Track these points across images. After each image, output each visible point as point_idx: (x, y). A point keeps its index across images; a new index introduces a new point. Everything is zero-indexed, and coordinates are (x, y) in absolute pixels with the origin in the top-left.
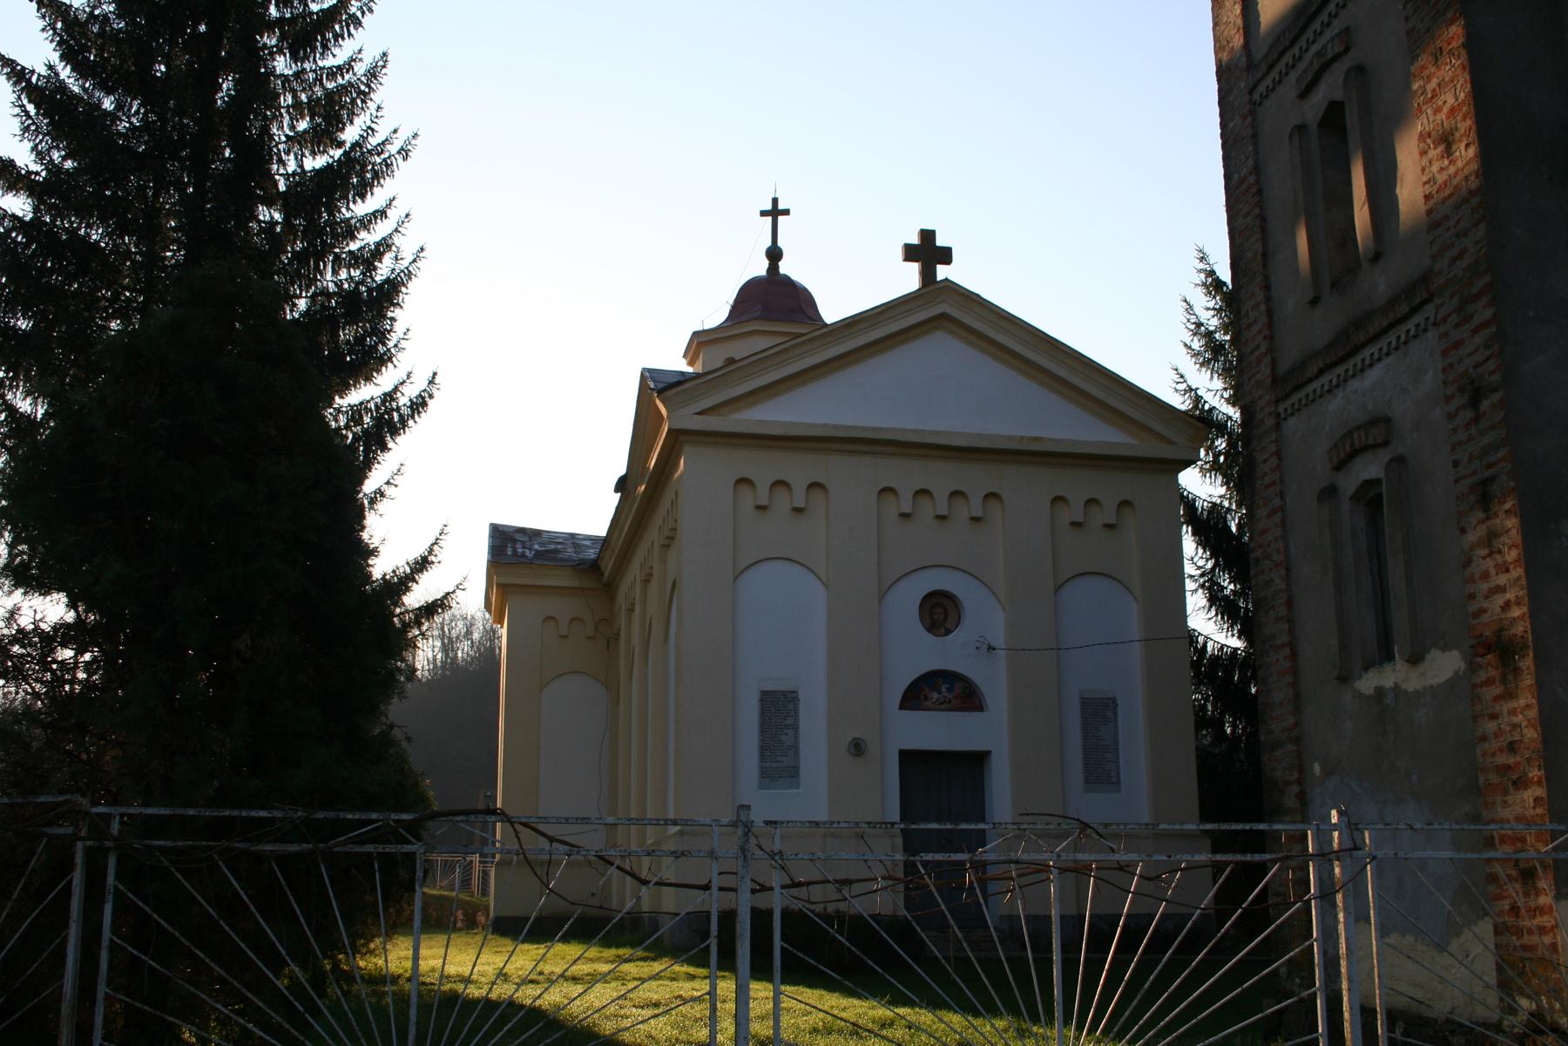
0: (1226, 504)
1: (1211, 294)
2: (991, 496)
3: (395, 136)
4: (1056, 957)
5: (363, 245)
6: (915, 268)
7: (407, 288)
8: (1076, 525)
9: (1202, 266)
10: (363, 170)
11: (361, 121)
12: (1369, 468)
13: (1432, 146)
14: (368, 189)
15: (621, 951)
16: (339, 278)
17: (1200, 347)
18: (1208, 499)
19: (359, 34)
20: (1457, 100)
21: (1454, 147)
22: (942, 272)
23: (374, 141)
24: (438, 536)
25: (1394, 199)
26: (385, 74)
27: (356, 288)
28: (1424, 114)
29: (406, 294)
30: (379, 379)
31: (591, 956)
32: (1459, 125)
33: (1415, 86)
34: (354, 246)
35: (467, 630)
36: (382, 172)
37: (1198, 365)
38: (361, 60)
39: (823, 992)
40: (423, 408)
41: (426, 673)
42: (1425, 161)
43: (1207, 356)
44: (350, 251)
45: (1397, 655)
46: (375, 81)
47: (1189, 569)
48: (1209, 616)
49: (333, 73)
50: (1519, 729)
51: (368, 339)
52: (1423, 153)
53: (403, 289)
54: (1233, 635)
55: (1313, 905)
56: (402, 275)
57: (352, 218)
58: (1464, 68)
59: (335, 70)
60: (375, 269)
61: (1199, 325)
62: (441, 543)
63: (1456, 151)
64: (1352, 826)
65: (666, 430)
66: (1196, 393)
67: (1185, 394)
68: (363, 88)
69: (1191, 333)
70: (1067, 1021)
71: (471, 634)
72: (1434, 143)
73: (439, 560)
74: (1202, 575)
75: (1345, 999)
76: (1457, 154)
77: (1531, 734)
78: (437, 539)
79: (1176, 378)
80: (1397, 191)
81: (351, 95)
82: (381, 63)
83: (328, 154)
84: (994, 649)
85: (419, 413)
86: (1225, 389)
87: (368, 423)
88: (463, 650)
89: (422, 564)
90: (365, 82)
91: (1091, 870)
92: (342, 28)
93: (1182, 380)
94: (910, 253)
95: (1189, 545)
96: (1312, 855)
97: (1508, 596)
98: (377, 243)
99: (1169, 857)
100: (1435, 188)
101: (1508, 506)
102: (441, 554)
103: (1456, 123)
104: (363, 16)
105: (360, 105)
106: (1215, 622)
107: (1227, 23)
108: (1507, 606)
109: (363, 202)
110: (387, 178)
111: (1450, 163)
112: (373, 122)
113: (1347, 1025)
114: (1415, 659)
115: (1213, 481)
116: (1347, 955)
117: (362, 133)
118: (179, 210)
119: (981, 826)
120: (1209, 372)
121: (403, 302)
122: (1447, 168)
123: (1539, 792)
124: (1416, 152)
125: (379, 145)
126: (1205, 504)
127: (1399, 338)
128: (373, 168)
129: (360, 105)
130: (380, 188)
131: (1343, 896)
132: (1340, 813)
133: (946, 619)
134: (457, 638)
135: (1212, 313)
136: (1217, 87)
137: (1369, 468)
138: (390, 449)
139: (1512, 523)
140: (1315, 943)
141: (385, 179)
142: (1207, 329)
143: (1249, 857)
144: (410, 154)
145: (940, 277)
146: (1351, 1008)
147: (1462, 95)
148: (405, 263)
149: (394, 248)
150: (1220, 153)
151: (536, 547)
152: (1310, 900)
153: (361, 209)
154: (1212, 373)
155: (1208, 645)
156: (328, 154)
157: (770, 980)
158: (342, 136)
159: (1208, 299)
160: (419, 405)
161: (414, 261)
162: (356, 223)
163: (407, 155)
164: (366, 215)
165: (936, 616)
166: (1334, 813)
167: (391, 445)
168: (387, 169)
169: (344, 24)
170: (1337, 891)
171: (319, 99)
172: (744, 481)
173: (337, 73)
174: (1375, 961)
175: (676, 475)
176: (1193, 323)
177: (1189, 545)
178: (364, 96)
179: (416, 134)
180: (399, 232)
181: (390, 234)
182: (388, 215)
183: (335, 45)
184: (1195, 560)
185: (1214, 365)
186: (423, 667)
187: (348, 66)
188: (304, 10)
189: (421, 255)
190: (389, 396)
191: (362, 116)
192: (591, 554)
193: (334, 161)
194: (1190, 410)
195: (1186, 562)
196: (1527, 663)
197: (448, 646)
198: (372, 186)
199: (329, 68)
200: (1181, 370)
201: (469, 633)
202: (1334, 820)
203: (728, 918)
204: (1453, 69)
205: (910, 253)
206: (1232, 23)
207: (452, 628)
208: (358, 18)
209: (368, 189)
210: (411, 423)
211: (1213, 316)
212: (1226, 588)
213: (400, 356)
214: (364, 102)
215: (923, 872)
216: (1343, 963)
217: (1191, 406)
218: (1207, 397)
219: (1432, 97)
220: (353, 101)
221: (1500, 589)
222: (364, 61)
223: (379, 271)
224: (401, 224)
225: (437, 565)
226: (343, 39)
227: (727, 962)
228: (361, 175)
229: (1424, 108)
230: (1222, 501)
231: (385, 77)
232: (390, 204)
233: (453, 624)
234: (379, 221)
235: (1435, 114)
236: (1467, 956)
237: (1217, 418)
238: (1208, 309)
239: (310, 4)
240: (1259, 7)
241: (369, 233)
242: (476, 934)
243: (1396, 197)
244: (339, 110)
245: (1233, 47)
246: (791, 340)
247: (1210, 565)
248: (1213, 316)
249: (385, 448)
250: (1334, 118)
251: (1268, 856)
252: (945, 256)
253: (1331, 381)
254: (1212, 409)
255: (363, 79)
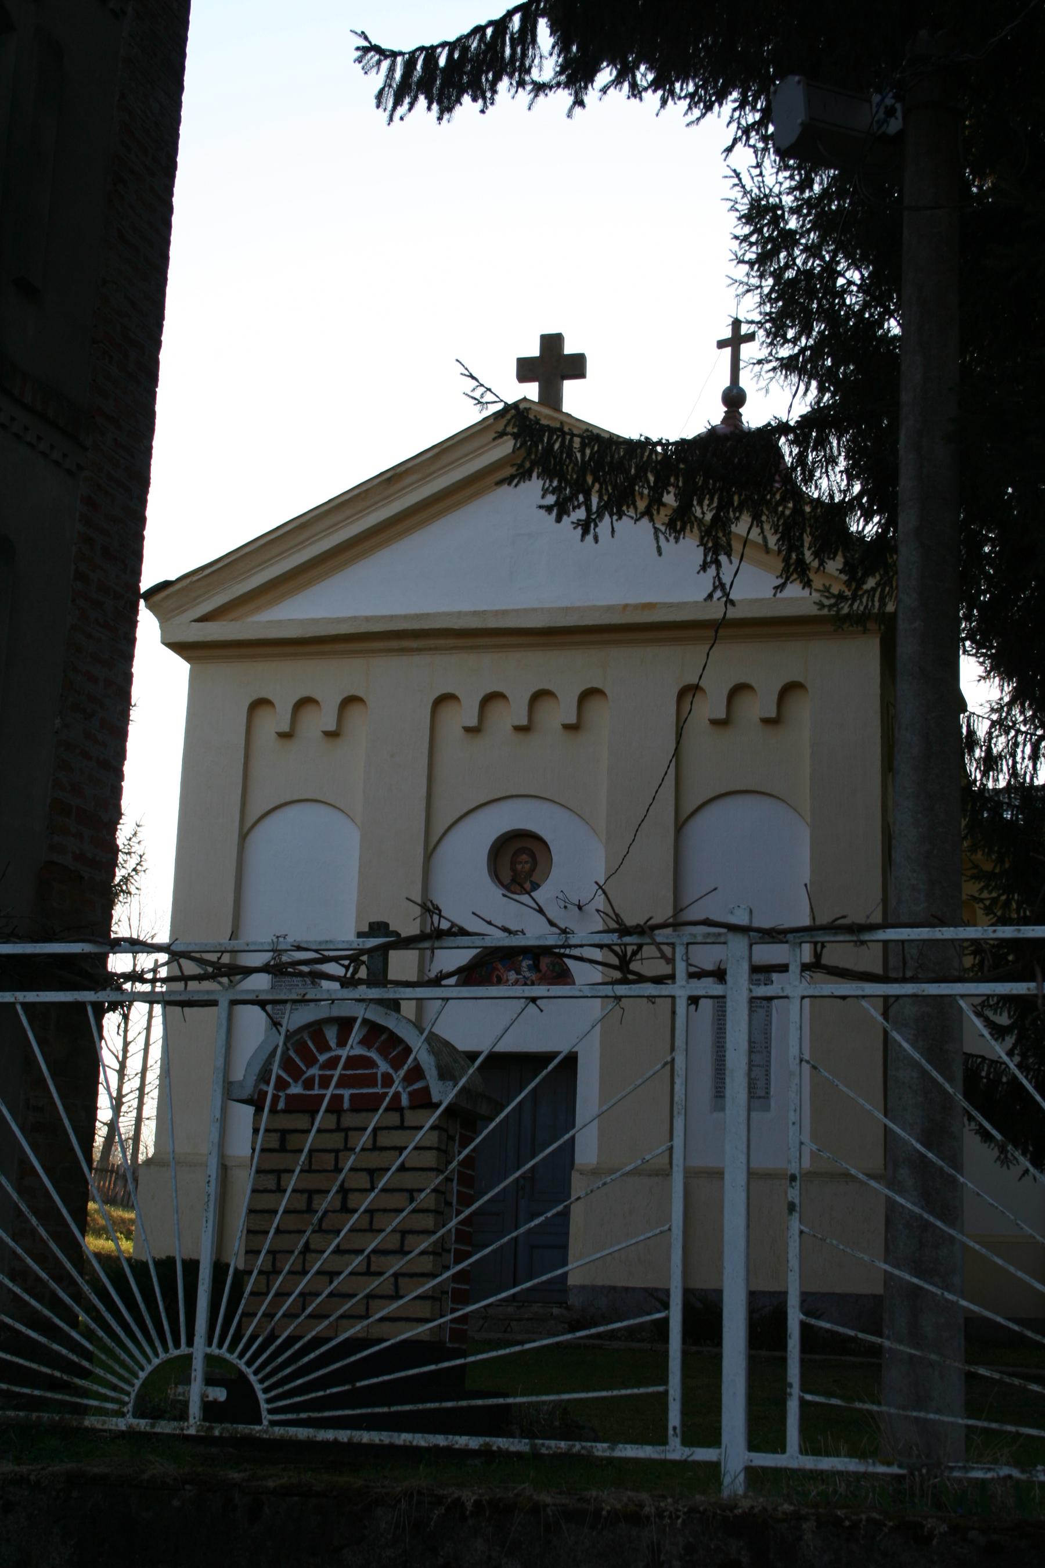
73: (143, 869)
118: (857, 472)
133: (533, 870)
165: (519, 867)
252: (576, 366)
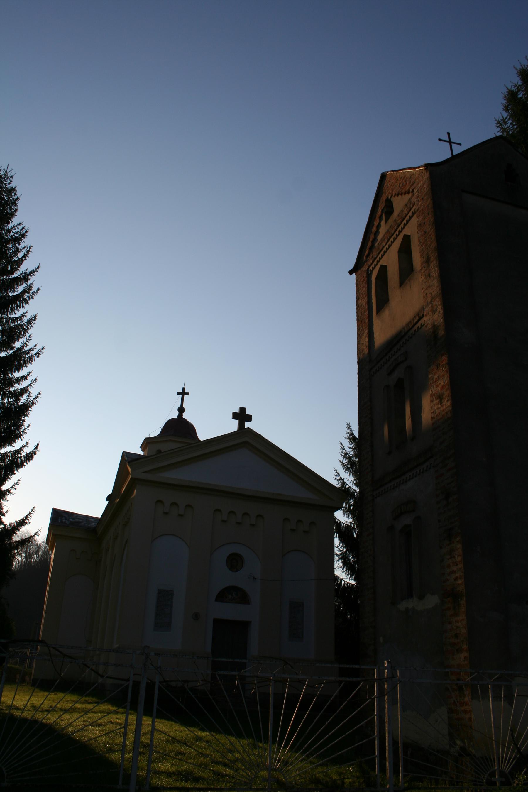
0: (352, 526)
1: (351, 442)
2: (259, 516)
3: (35, 347)
4: (271, 718)
5: (15, 389)
6: (236, 422)
7: (31, 409)
8: (292, 530)
9: (348, 431)
10: (20, 360)
11: (22, 340)
12: (407, 520)
13: (435, 399)
14: (21, 367)
15: (87, 699)
16: (4, 401)
17: (346, 462)
18: (346, 523)
19: (27, 307)
20: (444, 383)
21: (443, 401)
22: (247, 425)
23: (26, 349)
24: (30, 512)
25: (421, 418)
26: (34, 323)
27: (10, 407)
28: (433, 387)
29: (31, 411)
30: (15, 445)
31: (74, 700)
32: (445, 393)
33: (430, 376)
34: (12, 389)
35: (37, 550)
36: (28, 361)
37: (345, 470)
38: (26, 316)
39: (173, 723)
40: (31, 458)
41: (17, 567)
42: (432, 405)
43: (348, 466)
44: (10, 391)
45: (414, 596)
46: (30, 325)
47: (336, 551)
48: (343, 571)
49: (14, 320)
50: (459, 629)
51: (12, 428)
52: (432, 401)
53: (30, 409)
54: (352, 579)
55: (376, 700)
56: (30, 403)
57: (13, 378)
58: (447, 372)
59: (15, 319)
60: (19, 400)
61: (346, 454)
62: (32, 515)
63: (443, 402)
64: (392, 668)
65: (130, 477)
66: (343, 481)
67: (339, 481)
68: (25, 327)
69: (343, 457)
70: (274, 742)
71: (39, 552)
72: (436, 398)
73: (29, 522)
74: (341, 554)
75: (387, 741)
76: (444, 403)
77: (464, 631)
78: (30, 513)
79: (336, 474)
80: (422, 414)
81: (20, 329)
82: (33, 319)
83: (7, 352)
84: (256, 579)
85: (29, 460)
86: (355, 480)
87: (7, 462)
88: (34, 559)
89: (22, 523)
90: (26, 325)
91: (287, 682)
92: (20, 303)
93: (338, 475)
94: (235, 416)
95: (337, 541)
96: (376, 679)
97: (457, 575)
98: (21, 389)
99: (319, 677)
100: (436, 415)
101: (458, 539)
102: (31, 520)
103: (444, 392)
104: (29, 300)
105: (23, 334)
106: (345, 573)
107: (363, 344)
108: (456, 579)
109: (18, 372)
110: (29, 364)
111: (441, 406)
112: (27, 341)
113: (387, 752)
114: (421, 597)
115: (348, 516)
116: (388, 722)
117: (22, 345)
119: (244, 661)
120: (349, 473)
121: (29, 414)
122: (440, 408)
123: (466, 654)
124: (429, 401)
125: (28, 350)
126: (344, 525)
127: (420, 470)
128: (24, 359)
129: (23, 334)
130: (26, 367)
131: (388, 697)
132: (388, 662)
134: (33, 553)
135: (351, 449)
136: (357, 367)
137: (407, 520)
138: (15, 474)
139: (459, 546)
140: (376, 717)
141: (28, 364)
142: (349, 456)
143: (351, 679)
144: (40, 355)
145: (246, 427)
146: (389, 745)
147: (446, 382)
148: (32, 399)
149: (28, 392)
150: (357, 392)
151: (71, 520)
152: (374, 698)
153: (17, 375)
154: (350, 473)
155: (342, 582)
156: (7, 352)
157: (151, 716)
158: (13, 345)
159: (350, 444)
160: (30, 456)
161: (36, 398)
162: (14, 380)
163: (39, 356)
164: (19, 377)
166: (386, 662)
167: (16, 472)
168: (30, 360)
169: (21, 302)
170: (385, 695)
171: (7, 329)
172: (160, 502)
173: (15, 320)
174: (399, 725)
175: (132, 497)
176: (344, 453)
177: (337, 541)
178: (25, 331)
179: (43, 348)
180: (31, 386)
181: (27, 386)
182: (28, 378)
183: (16, 310)
184: (339, 548)
185: (351, 470)
186: (16, 564)
187: (20, 318)
188: (6, 294)
189: (39, 396)
190: (18, 451)
191: (23, 338)
192: (94, 525)
193: (9, 355)
194: (340, 487)
195: (335, 548)
196: (463, 602)
197: (28, 556)
198: (23, 366)
199: (12, 318)
200: (338, 471)
201: (38, 552)
202: (386, 665)
203: (137, 685)
204: (443, 372)
205: (235, 416)
206: (364, 344)
207: (31, 549)
208: (27, 300)
209: (21, 367)
210: (25, 464)
211: (352, 451)
212: (351, 560)
213: (24, 436)
214: (24, 333)
215: (218, 679)
216: (387, 725)
217: (341, 486)
218: (348, 482)
219: (436, 381)
220: (20, 332)
221: (454, 572)
222: (27, 317)
223: (21, 401)
224: (32, 382)
225: (28, 524)
226: (20, 308)
227: (134, 707)
228: (19, 361)
229: (433, 385)
230: (351, 524)
231: (34, 324)
232: (29, 374)
233: (32, 547)
234: (24, 380)
235: (436, 387)
236: (437, 721)
237: (351, 491)
238: (350, 448)
239: (9, 292)
240: (375, 340)
241: (19, 384)
242: (24, 686)
243: (421, 417)
244: (14, 335)
245: (364, 353)
246: (187, 446)
247: (345, 550)
248: (352, 451)
249: (13, 473)
250: (400, 383)
251: (359, 679)
252: (249, 418)
253: (394, 485)
254: (349, 487)
255: (25, 324)
